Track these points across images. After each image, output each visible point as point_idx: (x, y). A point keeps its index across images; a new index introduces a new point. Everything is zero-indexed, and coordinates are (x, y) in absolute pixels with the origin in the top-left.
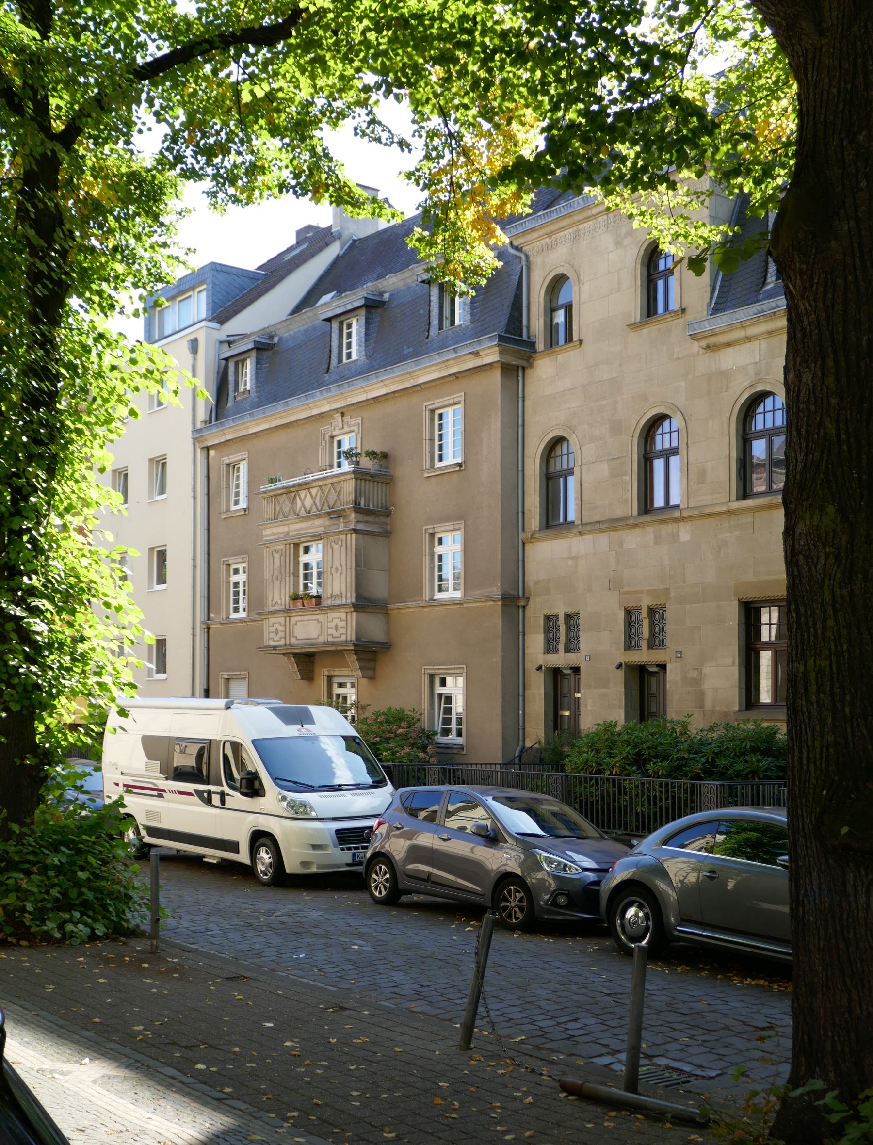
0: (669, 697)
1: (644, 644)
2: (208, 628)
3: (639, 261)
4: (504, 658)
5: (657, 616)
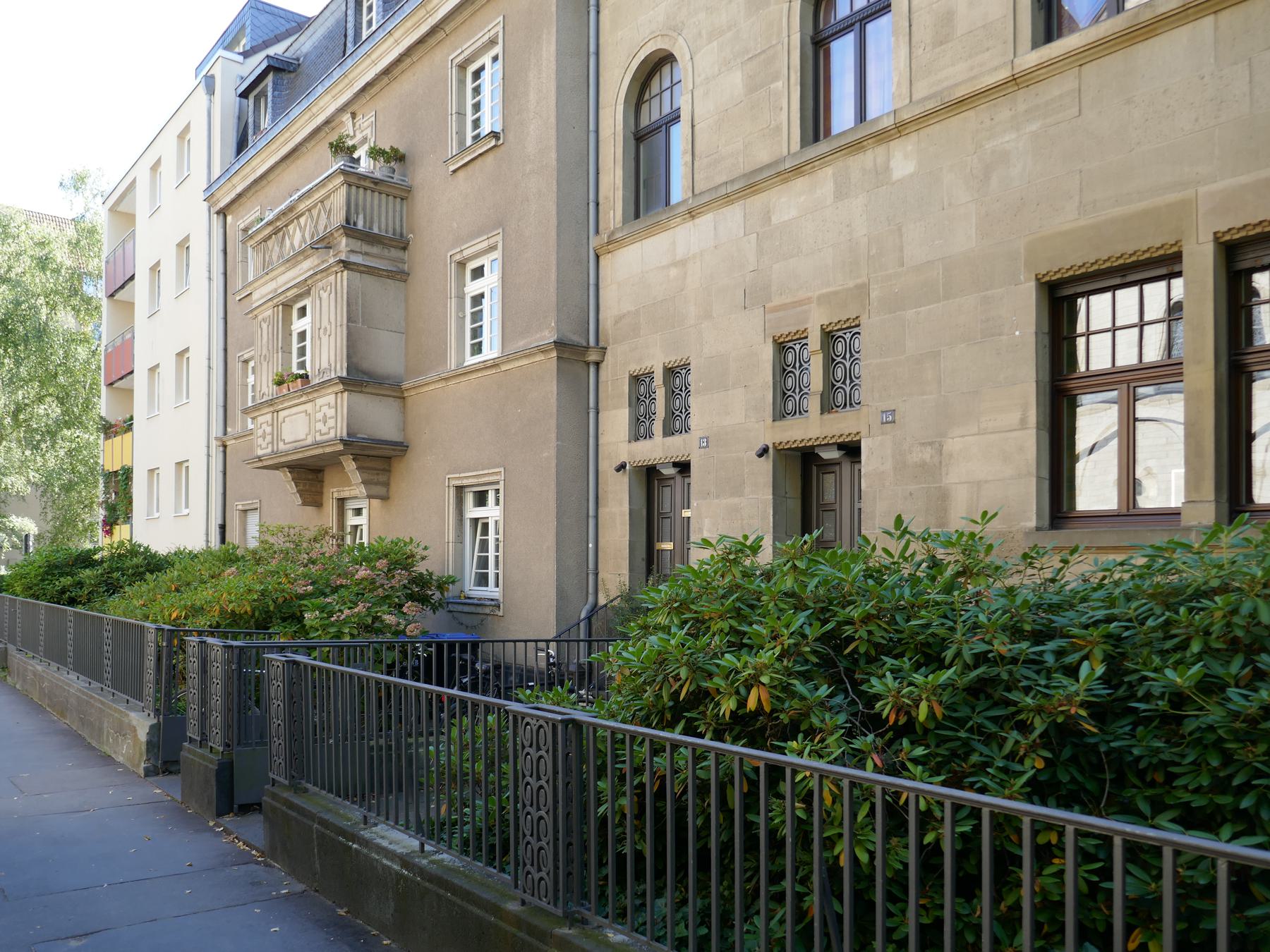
0: (865, 505)
1: (813, 404)
2: (225, 446)
4: (559, 449)
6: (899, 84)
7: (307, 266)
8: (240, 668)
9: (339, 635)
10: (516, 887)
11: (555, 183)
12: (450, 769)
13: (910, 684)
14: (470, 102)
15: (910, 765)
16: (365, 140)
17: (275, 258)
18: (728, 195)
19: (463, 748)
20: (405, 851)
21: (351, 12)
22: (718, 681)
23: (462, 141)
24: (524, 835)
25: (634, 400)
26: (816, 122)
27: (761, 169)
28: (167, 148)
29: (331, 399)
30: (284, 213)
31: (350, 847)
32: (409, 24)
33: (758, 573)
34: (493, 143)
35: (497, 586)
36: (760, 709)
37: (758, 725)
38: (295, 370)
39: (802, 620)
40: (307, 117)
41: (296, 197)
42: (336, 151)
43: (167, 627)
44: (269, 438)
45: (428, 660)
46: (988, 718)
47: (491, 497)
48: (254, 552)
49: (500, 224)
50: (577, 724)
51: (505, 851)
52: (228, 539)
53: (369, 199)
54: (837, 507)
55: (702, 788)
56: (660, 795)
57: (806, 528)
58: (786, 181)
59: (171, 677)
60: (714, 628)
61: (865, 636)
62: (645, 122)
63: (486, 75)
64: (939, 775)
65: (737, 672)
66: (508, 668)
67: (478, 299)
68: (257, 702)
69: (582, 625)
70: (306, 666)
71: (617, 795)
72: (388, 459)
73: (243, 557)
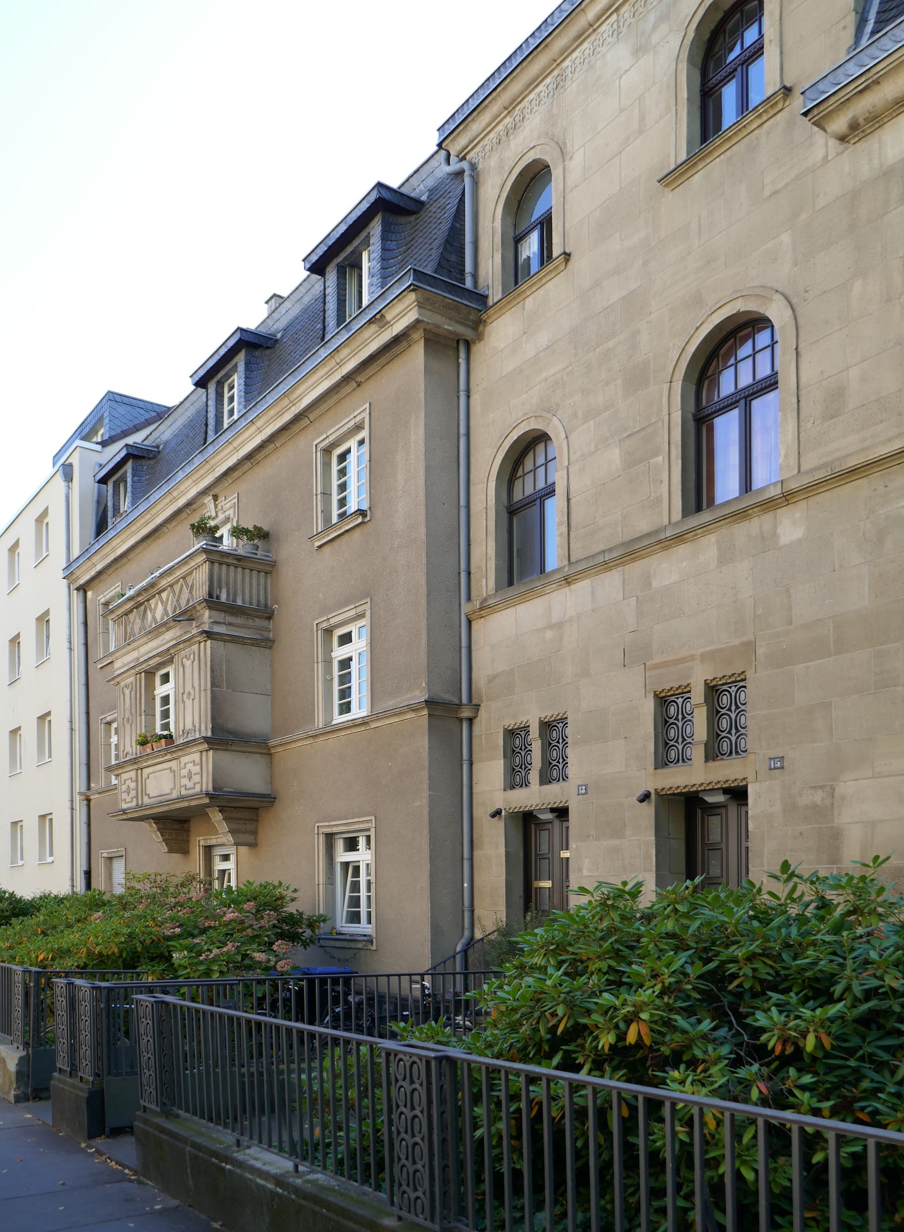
0: (753, 844)
2: (89, 801)
3: (684, 56)
4: (431, 799)
5: (725, 700)
6: (786, 456)
7: (168, 637)
8: (108, 1003)
9: (208, 973)
10: (392, 1203)
11: (424, 555)
12: (323, 1095)
13: (798, 1017)
14: (335, 483)
15: (797, 1092)
16: (227, 520)
17: (136, 629)
18: (605, 563)
19: (335, 1076)
20: (278, 1171)
21: (211, 403)
22: (596, 1017)
23: (327, 518)
24: (399, 1159)
25: (509, 752)
26: (698, 491)
27: (640, 538)
28: (26, 532)
29: (196, 757)
30: (145, 589)
31: (224, 1168)
32: (272, 413)
33: (638, 915)
34: (360, 520)
35: (369, 922)
36: (639, 1044)
37: (639, 1055)
38: (158, 731)
39: (683, 960)
40: (167, 500)
41: (157, 574)
42: (198, 531)
43: (34, 969)
44: (133, 793)
45: (299, 993)
46: (879, 1047)
47: (362, 842)
48: (121, 898)
49: (368, 594)
50: (452, 1062)
51: (380, 1168)
52: (93, 886)
53: (232, 574)
54: (723, 846)
55: (580, 1114)
56: (539, 1118)
57: (691, 876)
58: (667, 548)
59: (39, 1009)
60: (592, 968)
61: (750, 973)
62: (518, 496)
63: (352, 458)
64: (828, 1100)
65: (616, 1009)
66: (382, 997)
67: (345, 663)
68: (127, 1034)
69: (458, 957)
70: (175, 1006)
71: (493, 1120)
72: (256, 809)
73: (109, 902)
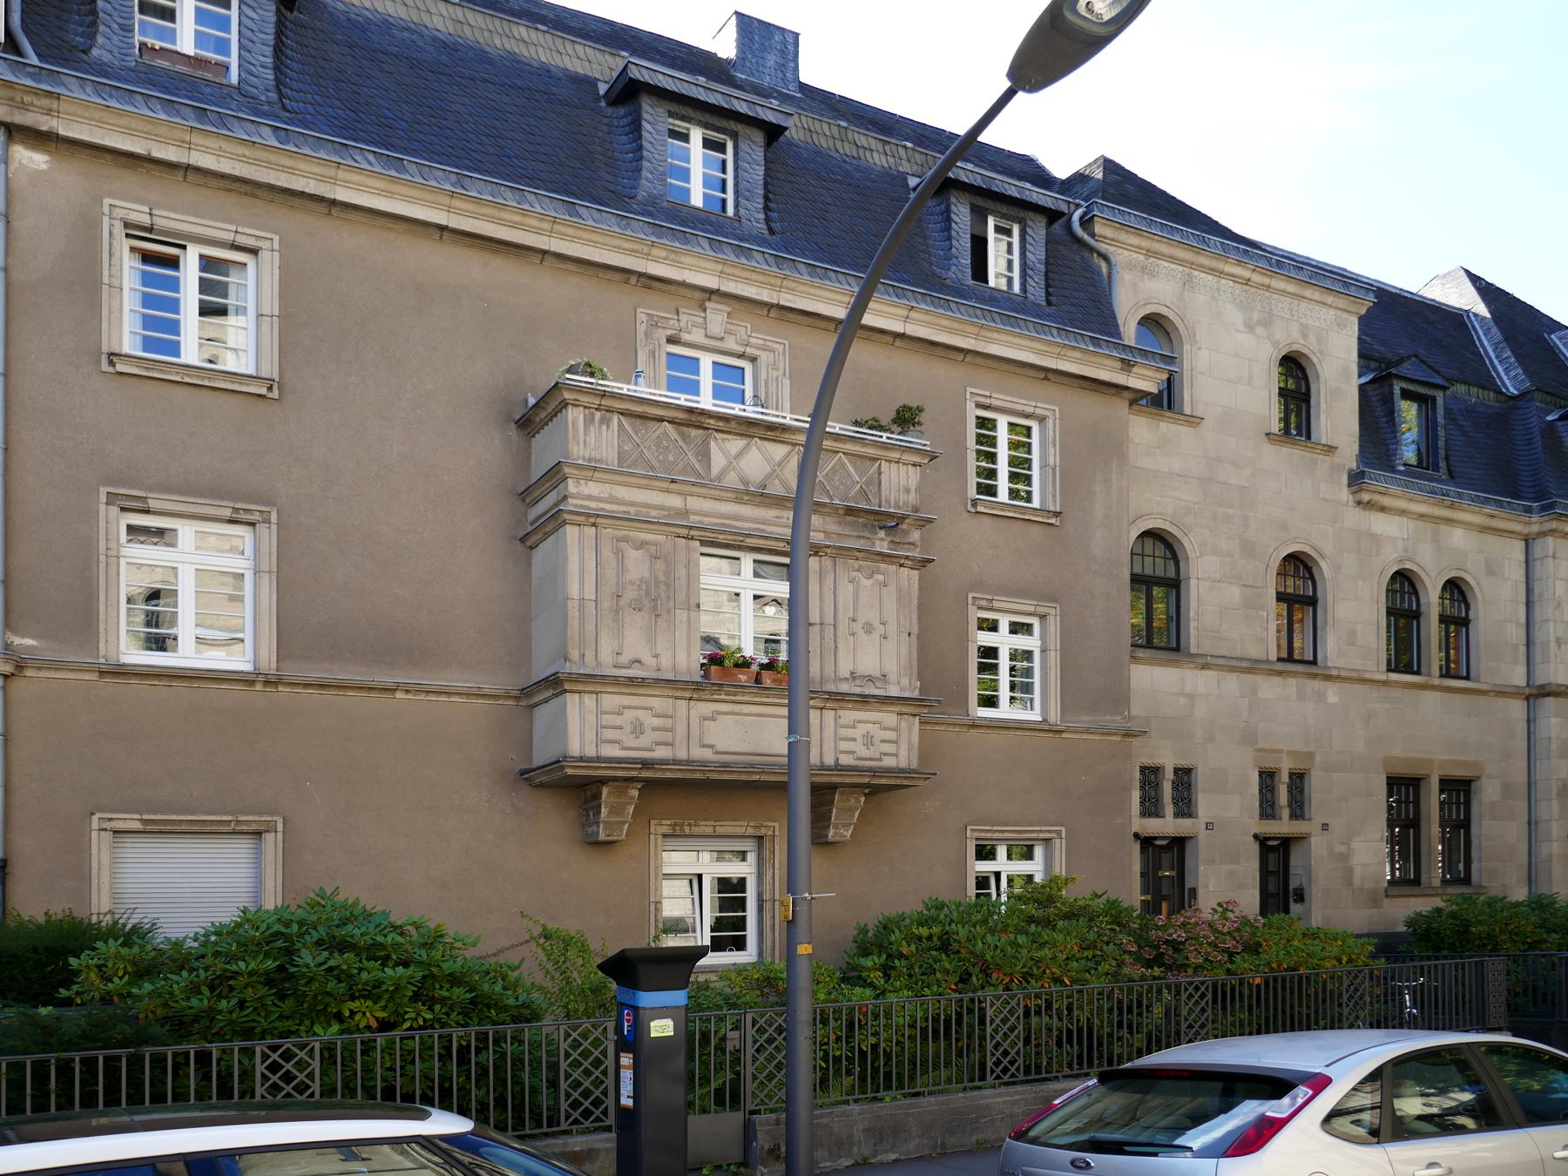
1: (1286, 813)
